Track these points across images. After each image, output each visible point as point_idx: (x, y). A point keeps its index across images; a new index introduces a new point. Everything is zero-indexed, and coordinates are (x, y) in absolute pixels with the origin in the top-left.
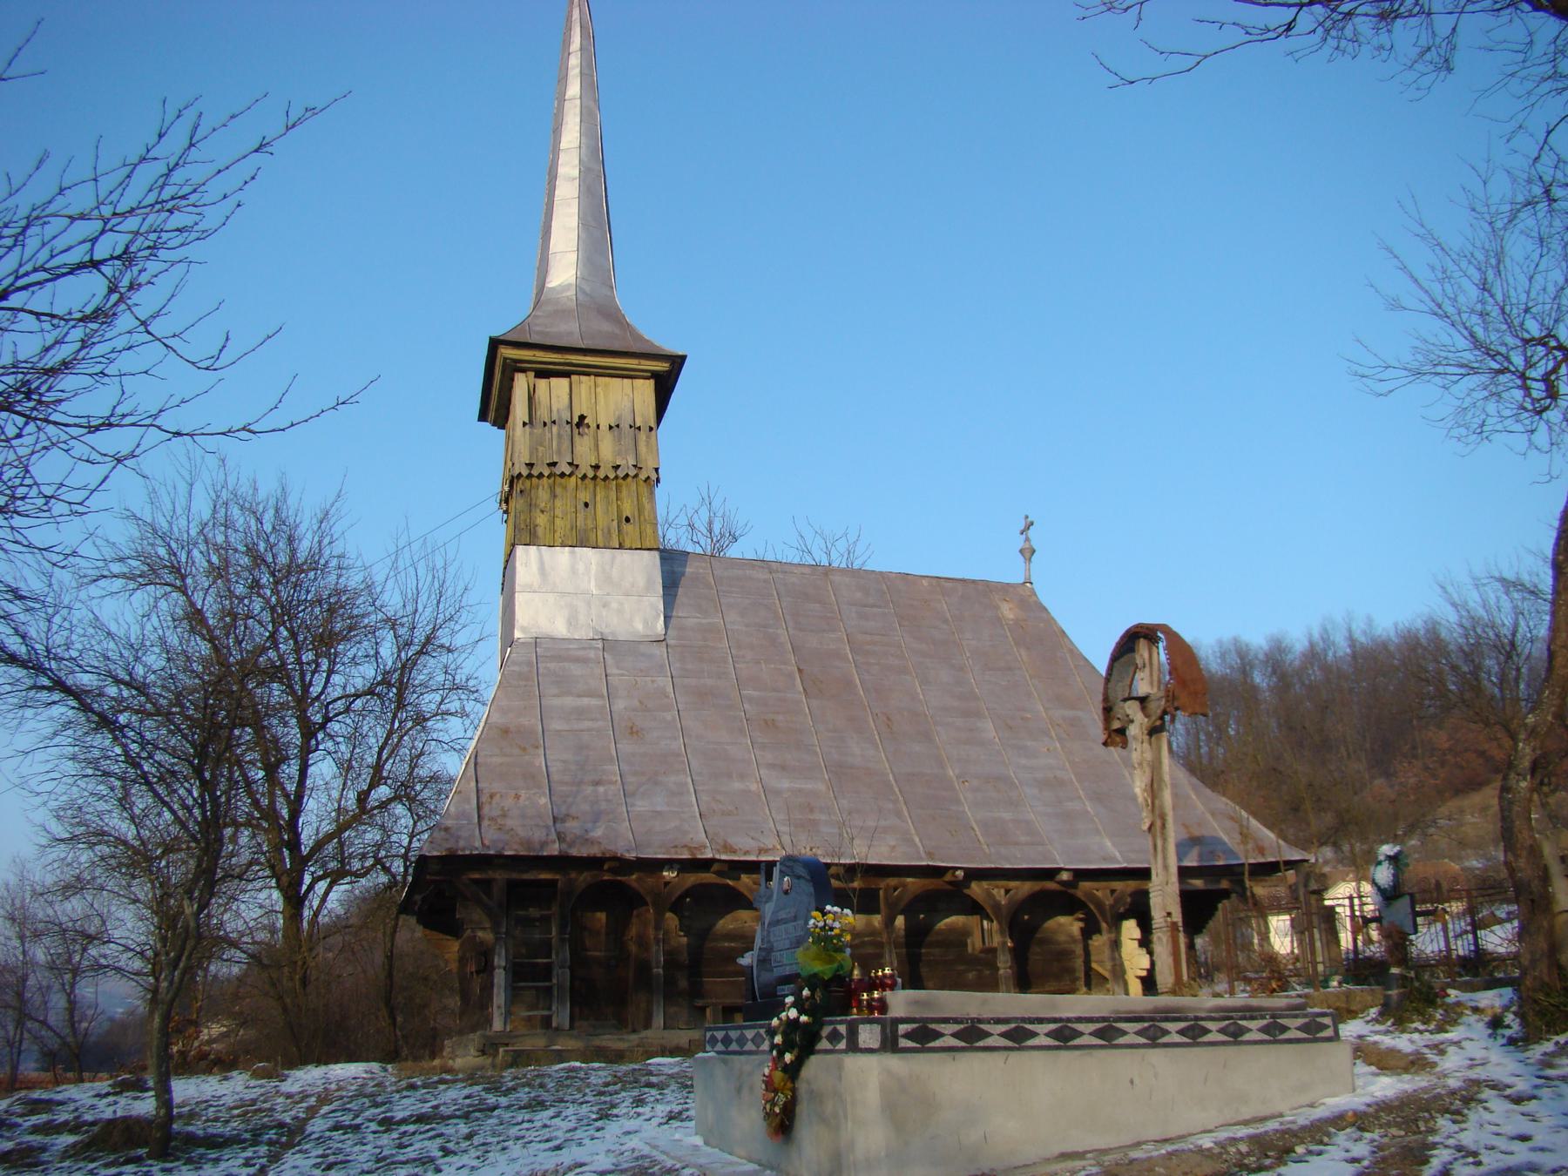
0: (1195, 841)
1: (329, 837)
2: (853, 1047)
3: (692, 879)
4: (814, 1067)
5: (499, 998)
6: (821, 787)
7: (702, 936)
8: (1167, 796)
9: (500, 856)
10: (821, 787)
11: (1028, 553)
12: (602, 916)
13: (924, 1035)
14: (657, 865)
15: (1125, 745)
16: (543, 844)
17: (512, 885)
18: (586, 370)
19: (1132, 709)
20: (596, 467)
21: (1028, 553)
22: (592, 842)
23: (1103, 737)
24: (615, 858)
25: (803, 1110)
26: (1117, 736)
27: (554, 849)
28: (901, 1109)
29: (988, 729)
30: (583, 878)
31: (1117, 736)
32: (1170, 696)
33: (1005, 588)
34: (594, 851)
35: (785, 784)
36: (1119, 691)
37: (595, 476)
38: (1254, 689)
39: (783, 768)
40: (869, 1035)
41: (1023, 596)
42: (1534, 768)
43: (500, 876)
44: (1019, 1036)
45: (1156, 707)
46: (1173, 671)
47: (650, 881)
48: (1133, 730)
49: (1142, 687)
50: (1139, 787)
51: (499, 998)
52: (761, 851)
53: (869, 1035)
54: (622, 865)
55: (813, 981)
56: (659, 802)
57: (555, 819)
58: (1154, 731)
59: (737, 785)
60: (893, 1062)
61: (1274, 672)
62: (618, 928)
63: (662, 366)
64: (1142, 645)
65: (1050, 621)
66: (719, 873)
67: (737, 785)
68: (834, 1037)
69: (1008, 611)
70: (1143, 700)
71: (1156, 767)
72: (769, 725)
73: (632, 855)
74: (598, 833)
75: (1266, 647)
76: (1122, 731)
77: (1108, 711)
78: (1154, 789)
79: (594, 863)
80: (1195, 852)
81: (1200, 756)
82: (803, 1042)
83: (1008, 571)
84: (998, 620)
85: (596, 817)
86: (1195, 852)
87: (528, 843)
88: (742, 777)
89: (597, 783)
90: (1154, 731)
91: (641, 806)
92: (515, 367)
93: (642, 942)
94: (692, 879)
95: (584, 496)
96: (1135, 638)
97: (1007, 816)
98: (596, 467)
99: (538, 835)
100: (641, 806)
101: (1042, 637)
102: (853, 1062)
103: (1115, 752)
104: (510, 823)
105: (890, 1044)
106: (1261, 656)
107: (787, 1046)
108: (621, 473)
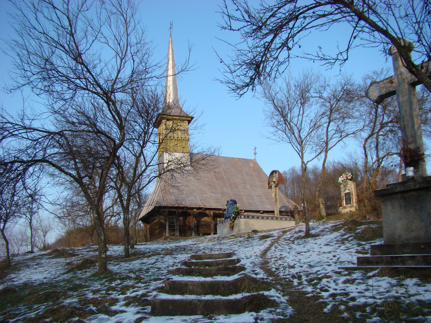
0: (284, 206)
1: (110, 207)
2: (241, 218)
3: (199, 211)
4: (236, 221)
5: (167, 230)
6: (220, 196)
7: (199, 221)
8: (277, 197)
9: (168, 206)
10: (220, 196)
11: (255, 154)
12: (182, 218)
13: (248, 217)
14: (193, 208)
15: (271, 189)
16: (175, 205)
17: (169, 211)
18: (176, 119)
19: (272, 183)
20: (178, 138)
21: (255, 154)
22: (183, 204)
23: (268, 187)
24: (187, 207)
25: (234, 226)
26: (270, 187)
27: (176, 205)
28: (246, 224)
29: (248, 186)
30: (181, 211)
31: (270, 187)
32: (278, 181)
33: (251, 161)
34: (182, 206)
35: (213, 195)
36: (271, 180)
37: (178, 140)
38: (310, 178)
39: (213, 192)
40: (242, 217)
41: (254, 162)
42: (319, 191)
43: (167, 210)
44: (258, 218)
45: (276, 183)
46: (279, 178)
47: (192, 211)
48: (273, 186)
49: (274, 180)
50: (273, 195)
51: (167, 230)
52: (211, 206)
53: (242, 217)
54: (188, 208)
55: (235, 212)
56: (193, 198)
57: (176, 201)
58: (276, 187)
59: (206, 195)
60: (245, 219)
61: (314, 174)
62: (184, 220)
63: (190, 119)
64: (274, 173)
65: (259, 167)
66: (203, 210)
67: (206, 195)
68: (239, 217)
69: (251, 165)
70: (274, 182)
71: (276, 192)
72: (210, 185)
73: (189, 207)
74: (183, 203)
75: (312, 168)
76: (271, 187)
77: (269, 183)
78: (275, 195)
79: (183, 208)
80: (284, 208)
81: (294, 196)
82: (235, 218)
83: (252, 157)
84: (250, 166)
85: (183, 200)
86: (284, 208)
87: (172, 204)
88: (206, 194)
89: (182, 195)
90: (276, 187)
91: (190, 199)
92: (164, 118)
93: (189, 223)
94: (199, 211)
95: (176, 143)
96: (273, 172)
97: (251, 201)
98: (178, 138)
99: (174, 203)
100: (190, 199)
101: (258, 170)
102: (241, 219)
103: (270, 190)
104: (168, 201)
105: (245, 218)
106: (311, 170)
107: (233, 219)
108: (182, 139)
